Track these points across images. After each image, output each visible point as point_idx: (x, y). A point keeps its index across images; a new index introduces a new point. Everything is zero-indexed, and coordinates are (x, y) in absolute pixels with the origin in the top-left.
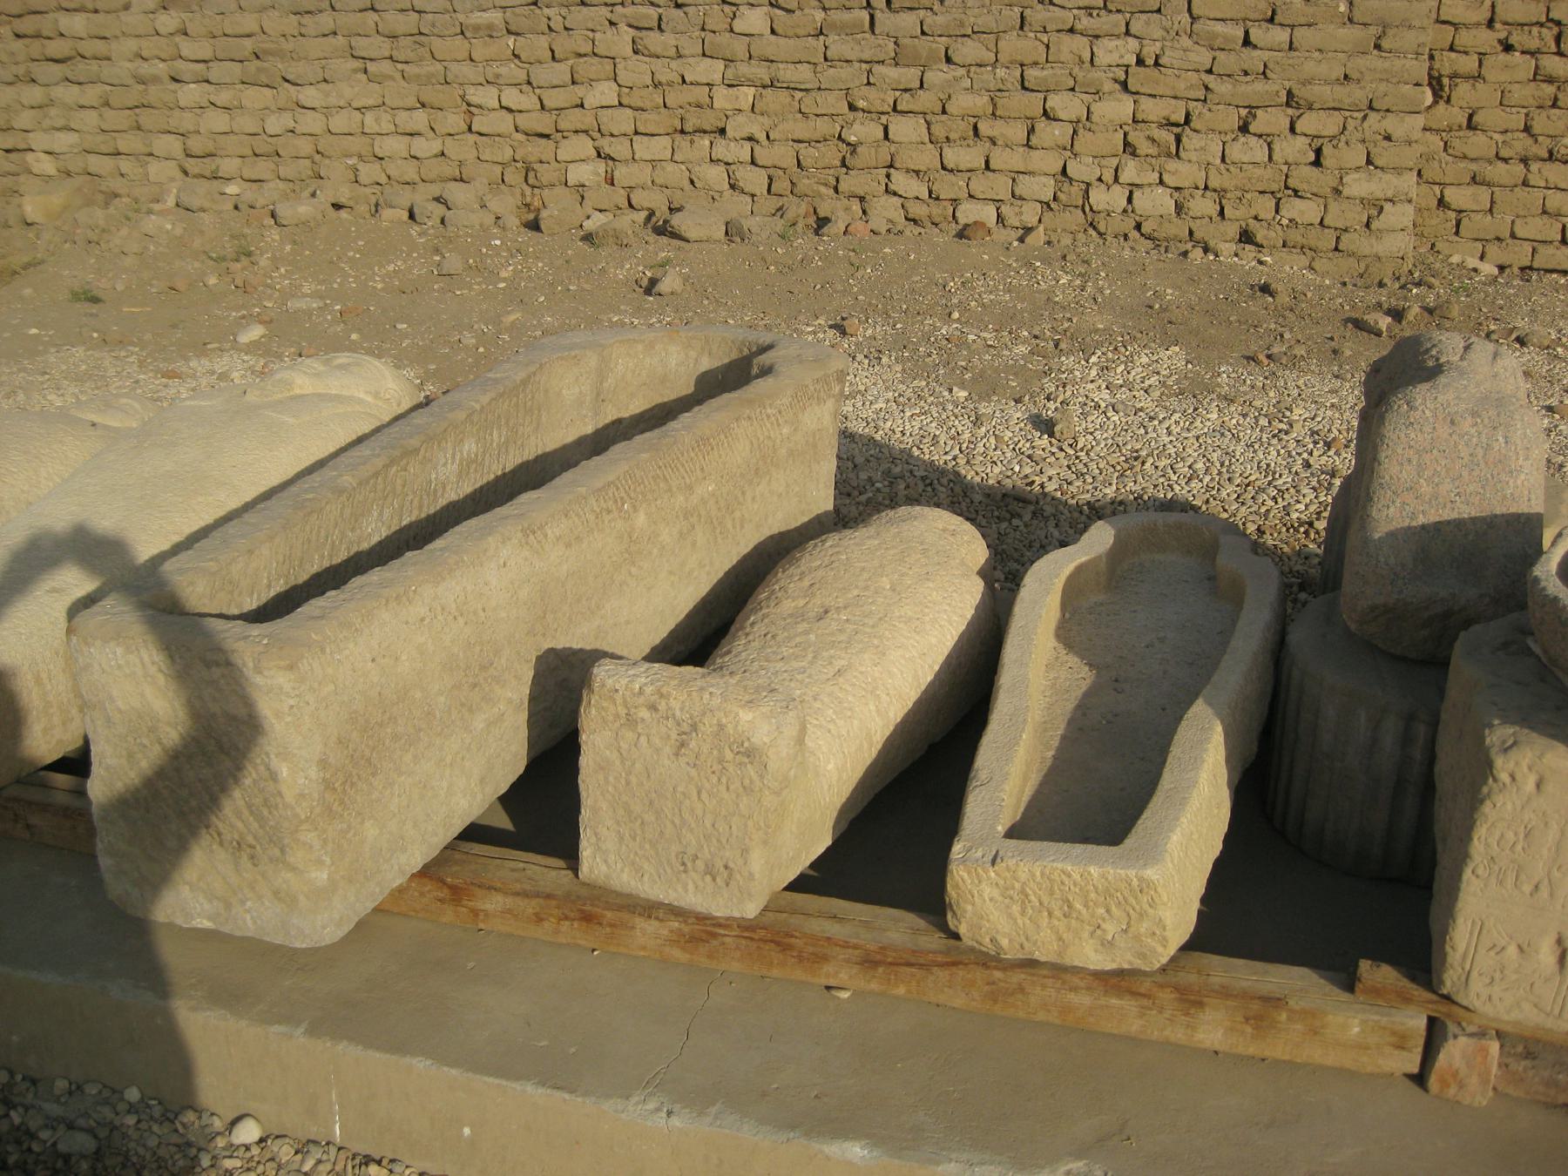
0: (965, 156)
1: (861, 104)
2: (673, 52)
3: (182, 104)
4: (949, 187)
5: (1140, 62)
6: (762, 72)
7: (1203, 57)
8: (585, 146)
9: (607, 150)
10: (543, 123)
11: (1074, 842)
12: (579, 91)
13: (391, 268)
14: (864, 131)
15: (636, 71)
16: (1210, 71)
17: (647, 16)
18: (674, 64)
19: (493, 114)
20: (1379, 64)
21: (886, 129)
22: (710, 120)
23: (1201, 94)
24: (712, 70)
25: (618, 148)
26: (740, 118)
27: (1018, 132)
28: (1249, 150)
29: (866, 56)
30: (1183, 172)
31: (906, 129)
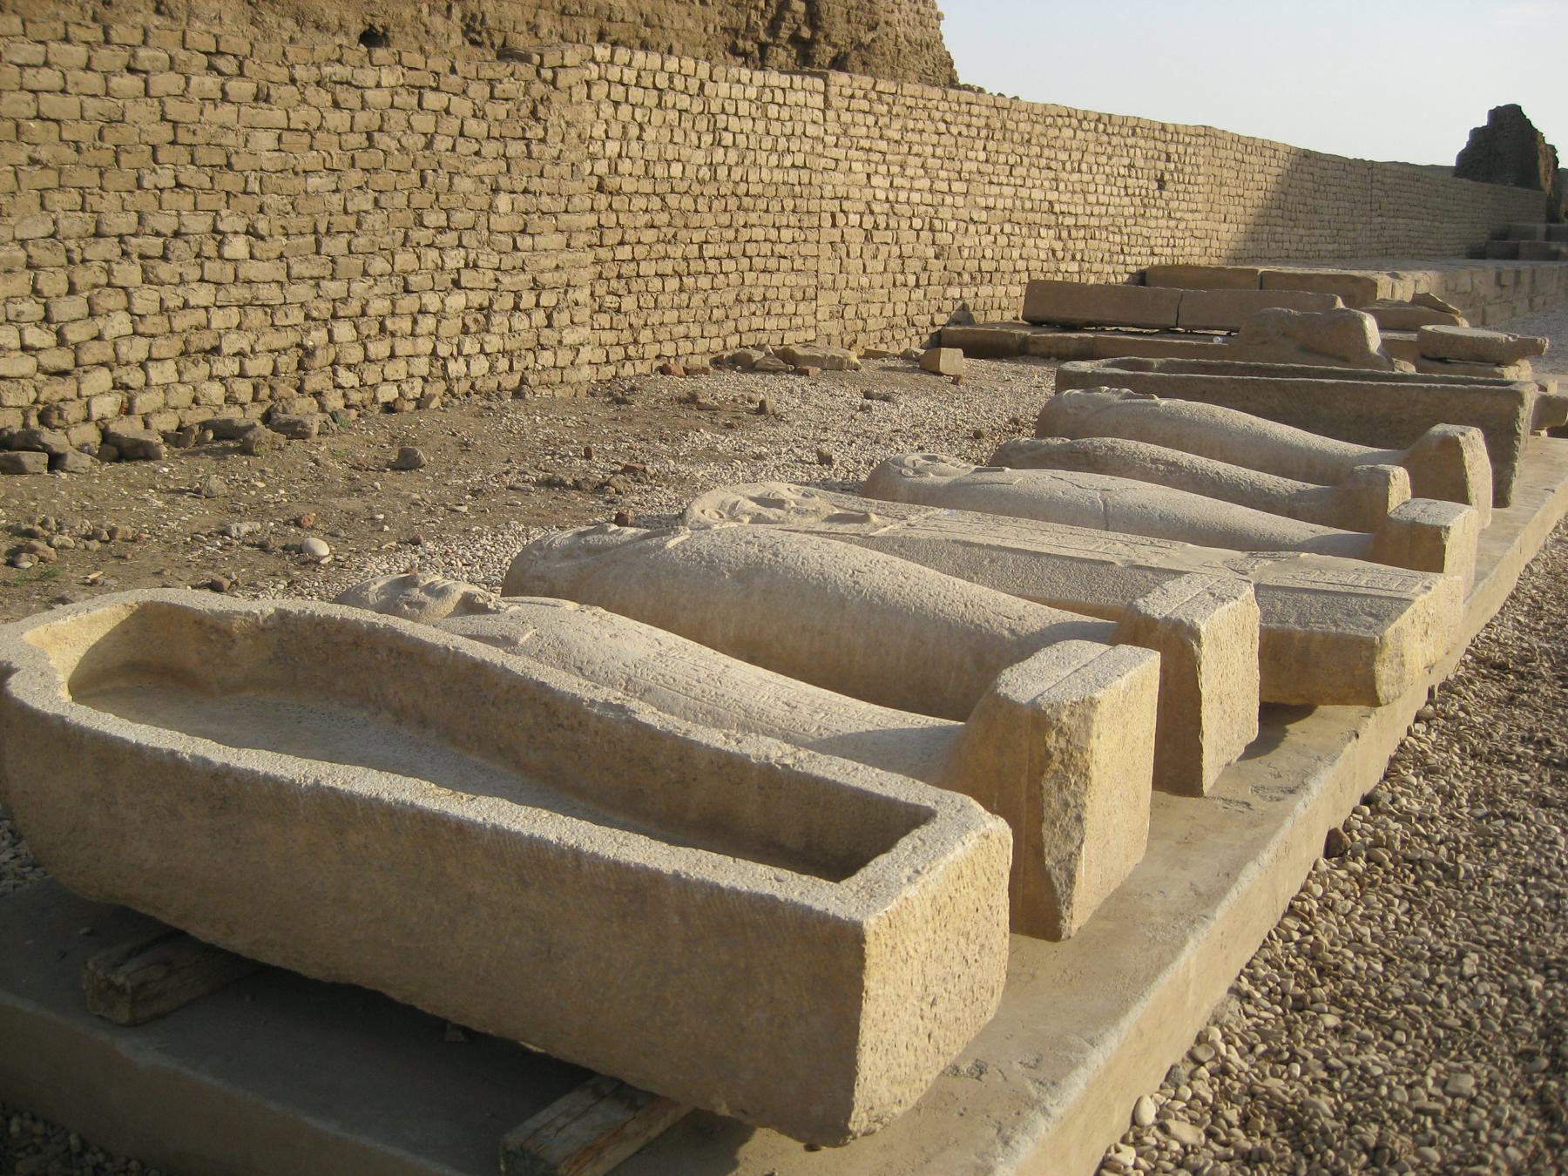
0: (379, 349)
1: (315, 314)
2: (177, 280)
3: (105, 370)
4: (372, 376)
5: (467, 266)
6: (239, 293)
7: (495, 260)
8: (103, 378)
9: (125, 379)
10: (63, 360)
11: (279, 969)
12: (100, 322)
13: (682, 468)
14: (317, 337)
15: (145, 300)
16: (498, 269)
17: (154, 245)
18: (180, 291)
19: (14, 354)
20: (571, 256)
21: (330, 332)
22: (208, 341)
23: (493, 285)
24: (202, 295)
25: (135, 378)
26: (233, 336)
27: (406, 325)
28: (520, 322)
29: (315, 273)
30: (493, 343)
31: (344, 331)
